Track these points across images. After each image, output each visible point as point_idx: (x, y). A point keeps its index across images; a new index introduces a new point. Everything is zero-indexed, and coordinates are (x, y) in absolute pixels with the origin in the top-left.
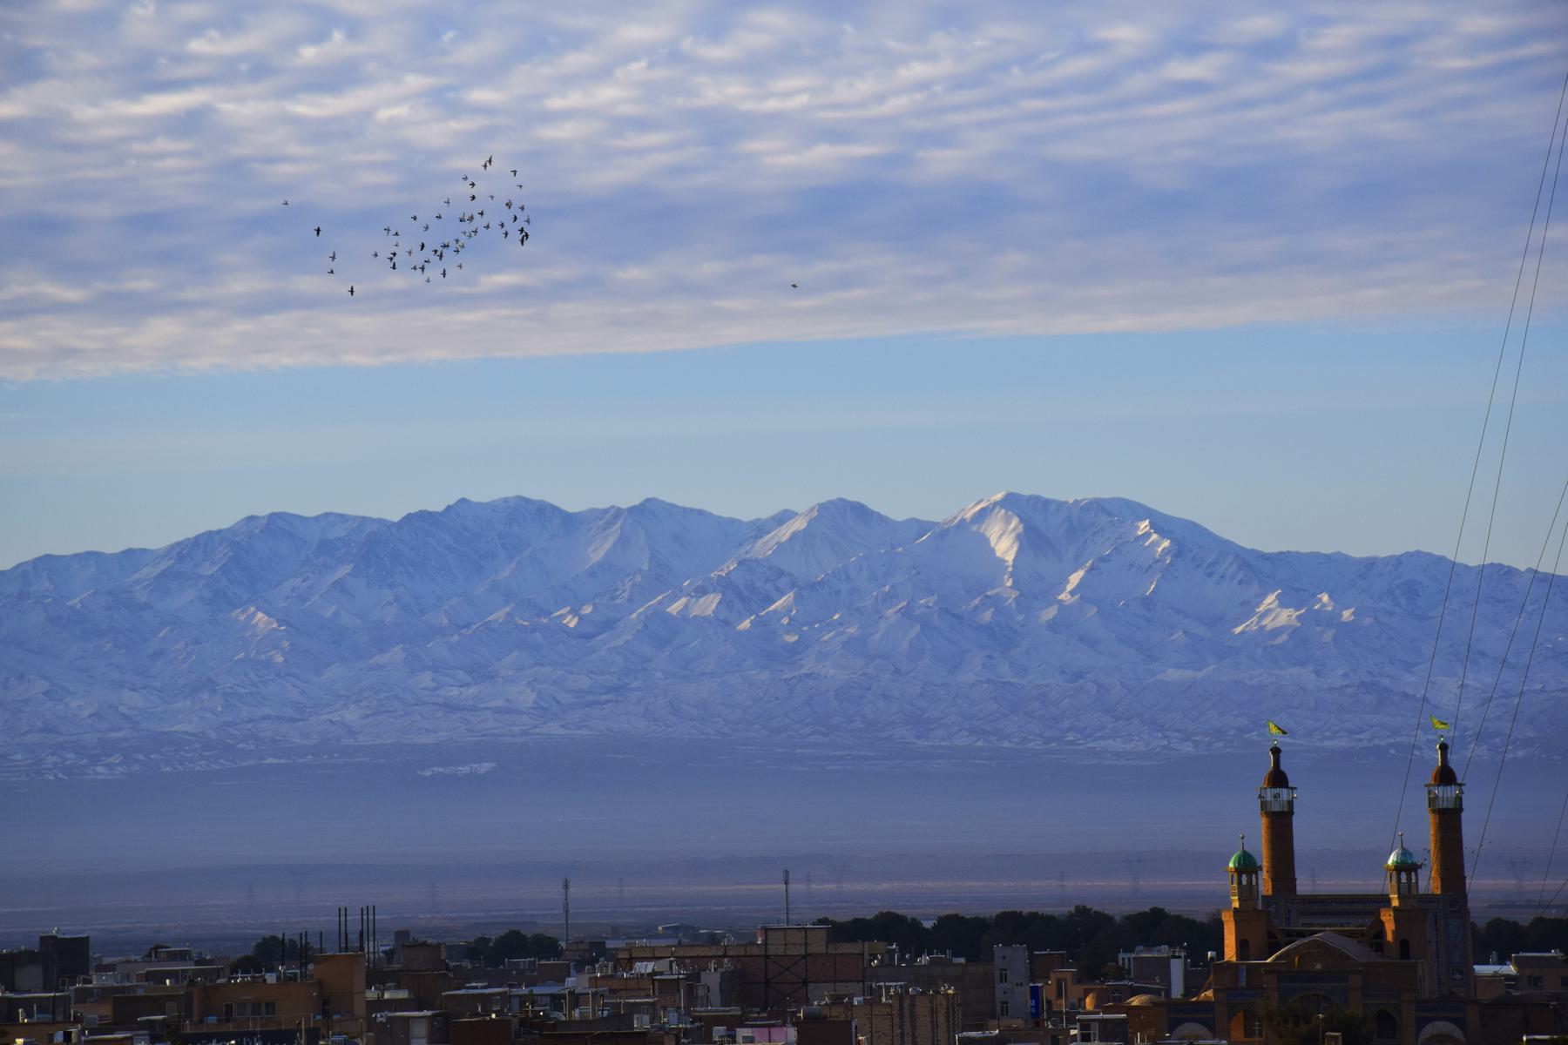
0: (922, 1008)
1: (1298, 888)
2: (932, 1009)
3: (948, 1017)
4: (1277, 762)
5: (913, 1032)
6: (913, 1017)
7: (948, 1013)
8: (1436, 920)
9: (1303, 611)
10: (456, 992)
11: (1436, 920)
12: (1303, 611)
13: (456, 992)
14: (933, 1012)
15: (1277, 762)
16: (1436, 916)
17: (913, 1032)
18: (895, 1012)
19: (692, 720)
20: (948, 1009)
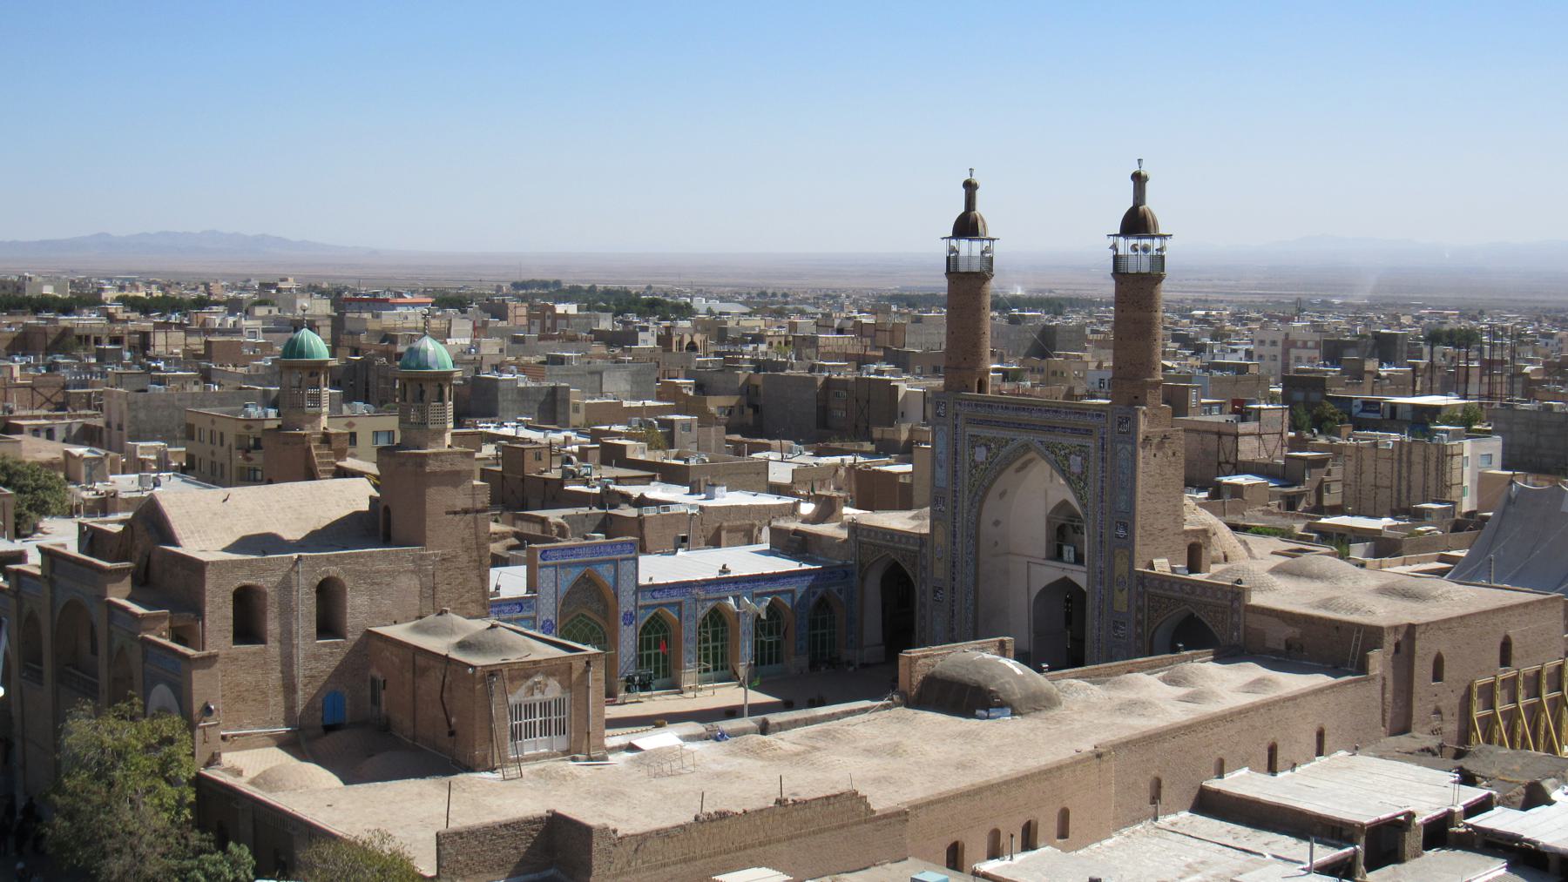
0: (1417, 457)
1: (364, 509)
2: (1425, 457)
3: (1437, 466)
4: (970, 202)
5: (1409, 477)
6: (1410, 463)
7: (1438, 461)
8: (1103, 445)
9: (138, 610)
10: (417, 451)
11: (1103, 445)
12: (138, 610)
13: (417, 451)
14: (1426, 459)
15: (970, 202)
16: (1103, 438)
17: (1409, 477)
18: (1396, 457)
19: (528, 677)
20: (1438, 458)
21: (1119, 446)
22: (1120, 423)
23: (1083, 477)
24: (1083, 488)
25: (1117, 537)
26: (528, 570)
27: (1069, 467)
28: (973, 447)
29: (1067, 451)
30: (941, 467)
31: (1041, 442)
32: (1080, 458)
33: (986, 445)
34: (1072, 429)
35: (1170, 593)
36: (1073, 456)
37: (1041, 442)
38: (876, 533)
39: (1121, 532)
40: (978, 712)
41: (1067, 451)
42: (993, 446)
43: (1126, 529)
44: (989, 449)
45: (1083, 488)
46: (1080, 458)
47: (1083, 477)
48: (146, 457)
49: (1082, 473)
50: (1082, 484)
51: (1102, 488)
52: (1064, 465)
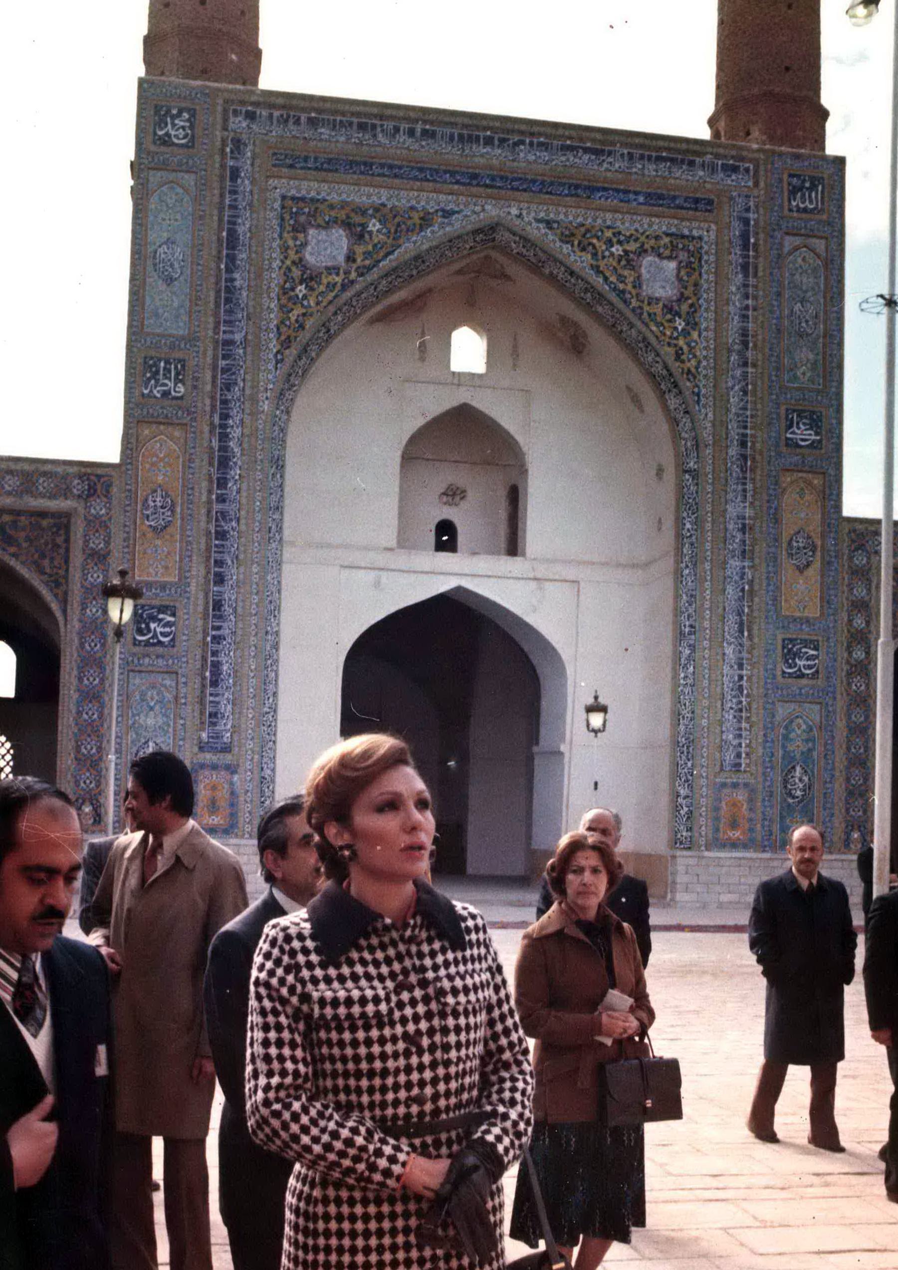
16: (746, 222)
21: (789, 242)
22: (793, 191)
23: (685, 307)
24: (686, 333)
25: (792, 444)
26: (838, 507)
27: (638, 284)
28: (299, 229)
29: (632, 246)
30: (169, 281)
31: (549, 224)
32: (673, 265)
33: (347, 225)
34: (648, 195)
35: (77, 558)
36: (649, 260)
37: (549, 224)
38: (134, 333)
39: (803, 434)
40: (774, 989)
41: (632, 246)
42: (374, 226)
43: (815, 423)
44: (358, 234)
45: (686, 333)
46: (673, 265)
47: (685, 307)
48: (166, 579)
49: (682, 298)
50: (680, 324)
51: (744, 333)
52: (622, 279)
